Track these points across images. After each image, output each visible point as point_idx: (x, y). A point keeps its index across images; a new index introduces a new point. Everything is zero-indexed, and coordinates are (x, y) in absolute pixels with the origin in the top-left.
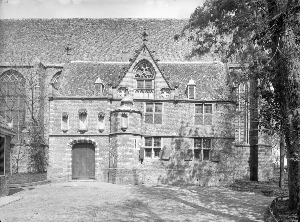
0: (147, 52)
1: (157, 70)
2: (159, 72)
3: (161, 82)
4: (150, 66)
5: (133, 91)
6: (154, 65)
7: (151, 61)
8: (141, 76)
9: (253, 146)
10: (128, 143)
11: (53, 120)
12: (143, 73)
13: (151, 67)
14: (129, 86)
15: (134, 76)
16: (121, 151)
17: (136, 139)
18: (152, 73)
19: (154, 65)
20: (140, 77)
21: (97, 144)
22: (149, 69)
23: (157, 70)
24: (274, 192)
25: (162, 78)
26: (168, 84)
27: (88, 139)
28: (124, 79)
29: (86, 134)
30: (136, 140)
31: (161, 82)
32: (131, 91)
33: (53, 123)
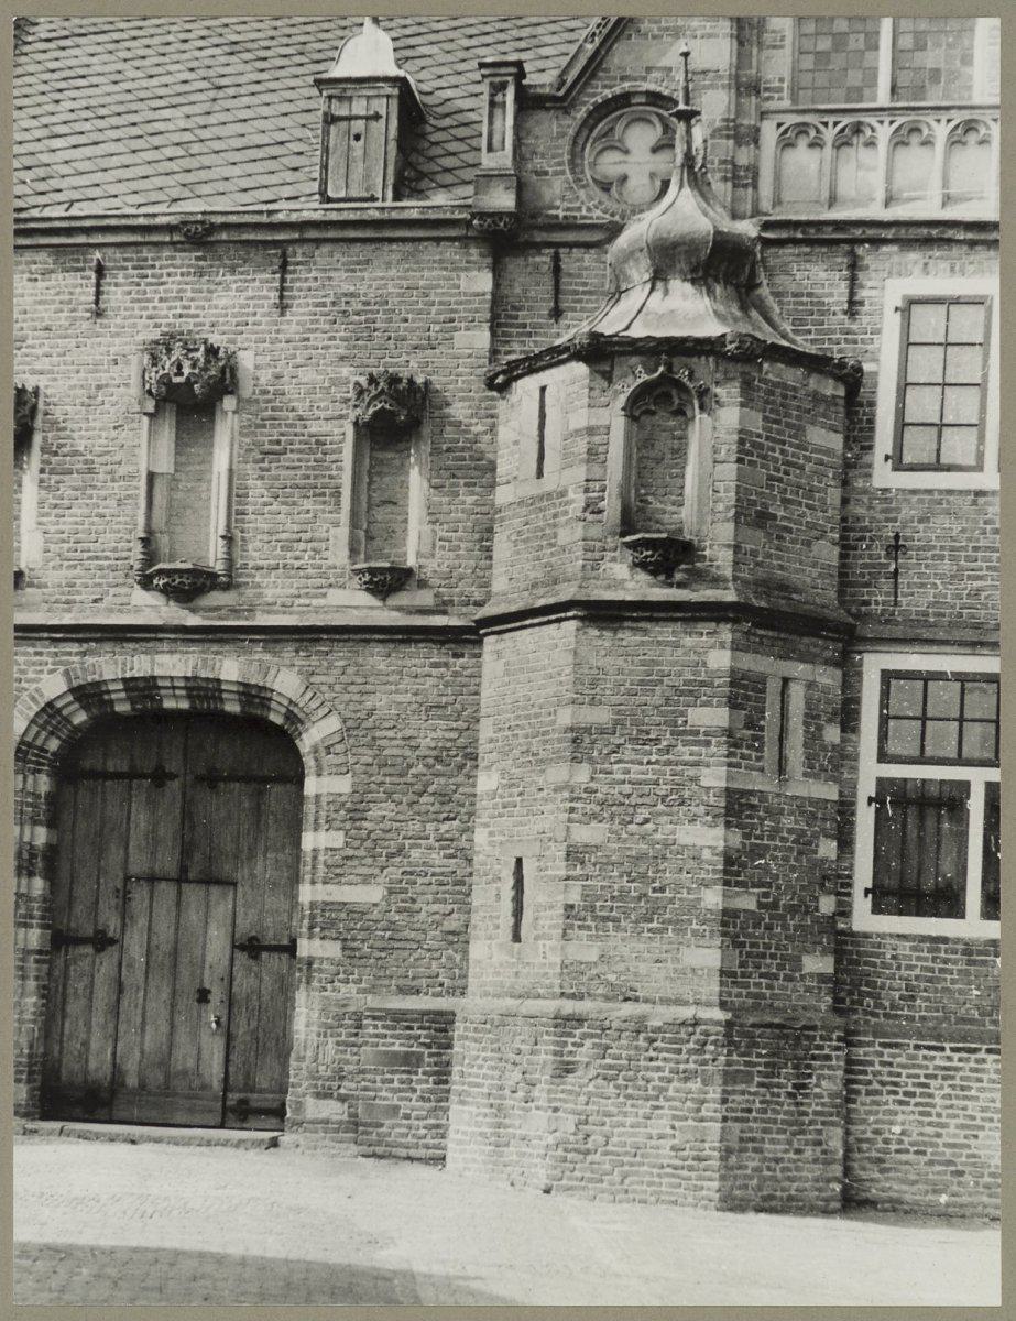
5: (754, 137)
29: (215, 608)
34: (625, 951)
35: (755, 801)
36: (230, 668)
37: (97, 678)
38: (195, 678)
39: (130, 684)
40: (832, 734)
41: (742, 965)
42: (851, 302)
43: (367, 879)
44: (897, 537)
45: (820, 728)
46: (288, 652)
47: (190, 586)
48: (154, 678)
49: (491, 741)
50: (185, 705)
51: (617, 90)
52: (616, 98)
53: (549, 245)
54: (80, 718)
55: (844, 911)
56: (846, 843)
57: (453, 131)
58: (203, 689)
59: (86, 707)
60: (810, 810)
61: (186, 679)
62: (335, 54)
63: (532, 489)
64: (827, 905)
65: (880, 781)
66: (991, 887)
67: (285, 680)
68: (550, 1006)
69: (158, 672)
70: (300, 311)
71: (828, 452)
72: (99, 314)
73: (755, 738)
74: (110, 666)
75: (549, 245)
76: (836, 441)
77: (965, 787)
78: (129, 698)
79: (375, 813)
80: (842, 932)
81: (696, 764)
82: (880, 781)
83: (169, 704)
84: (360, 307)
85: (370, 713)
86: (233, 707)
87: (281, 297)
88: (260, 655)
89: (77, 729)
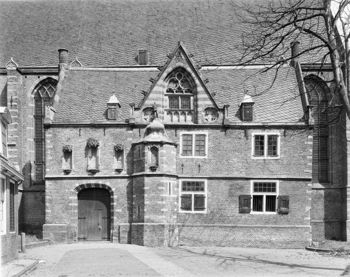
1: (197, 82)
6: (193, 75)
8: (175, 91)
10: (160, 188)
12: (178, 86)
14: (158, 106)
15: (165, 90)
16: (150, 199)
18: (190, 86)
19: (193, 75)
20: (173, 92)
23: (197, 82)
29: (97, 175)
31: (205, 99)
34: (152, 217)
35: (166, 198)
36: (100, 182)
37: (83, 184)
38: (96, 184)
39: (87, 184)
40: (176, 189)
41: (166, 218)
42: (176, 135)
43: (119, 208)
44: (183, 164)
45: (174, 188)
46: (108, 180)
47: (93, 172)
48: (90, 184)
49: (134, 191)
50: (94, 187)
51: (147, 107)
52: (146, 108)
53: (139, 127)
54: (81, 189)
55: (178, 210)
56: (178, 202)
57: (125, 109)
58: (97, 185)
59: (81, 188)
60: (174, 198)
61: (95, 184)
62: (109, 98)
63: (138, 159)
64: (176, 210)
65: (266, 211)
66: (303, 102)
67: (108, 183)
68: (144, 224)
69: (91, 183)
70: (107, 136)
71: (174, 154)
72: (80, 135)
73: (167, 190)
74: (85, 182)
75: (139, 127)
76: (175, 153)
77: (191, 195)
78: (87, 186)
79: (120, 200)
80: (178, 213)
81: (160, 194)
82: (266, 211)
83: (92, 187)
84: (115, 135)
85: (119, 187)
86: (101, 187)
87: (104, 133)
88: (104, 180)
89: (80, 190)
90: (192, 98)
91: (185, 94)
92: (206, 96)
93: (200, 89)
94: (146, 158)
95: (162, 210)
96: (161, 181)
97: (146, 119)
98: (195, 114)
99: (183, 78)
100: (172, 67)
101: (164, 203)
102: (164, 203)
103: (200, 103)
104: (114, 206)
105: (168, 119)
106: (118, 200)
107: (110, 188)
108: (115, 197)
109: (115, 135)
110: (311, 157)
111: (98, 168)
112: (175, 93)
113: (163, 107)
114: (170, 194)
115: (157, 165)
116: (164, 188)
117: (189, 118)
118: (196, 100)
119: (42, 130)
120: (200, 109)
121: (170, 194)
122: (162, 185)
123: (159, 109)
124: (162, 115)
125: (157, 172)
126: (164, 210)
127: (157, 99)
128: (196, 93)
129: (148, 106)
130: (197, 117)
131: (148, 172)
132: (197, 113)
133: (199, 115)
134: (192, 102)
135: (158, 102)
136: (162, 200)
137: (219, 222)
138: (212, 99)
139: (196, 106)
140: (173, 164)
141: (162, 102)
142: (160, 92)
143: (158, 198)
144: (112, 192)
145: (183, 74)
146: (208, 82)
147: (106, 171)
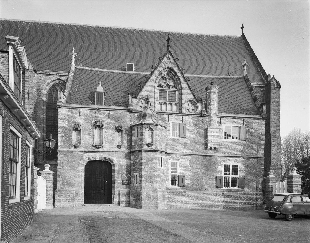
0: (172, 60)
1: (182, 80)
2: (185, 82)
3: (188, 94)
4: (174, 75)
6: (179, 74)
7: (176, 70)
9: (281, 165)
10: (155, 161)
11: (63, 132)
13: (174, 76)
14: (151, 97)
15: (156, 85)
16: (147, 171)
17: (163, 157)
18: (175, 83)
19: (179, 74)
20: (162, 87)
21: (115, 162)
22: (173, 79)
23: (182, 80)
24: (153, 84)
25: (191, 95)
26: (194, 96)
27: (105, 155)
28: (145, 88)
29: (100, 150)
30: (137, 176)
31: (188, 94)
32: (153, 102)
33: (62, 137)
50: (99, 160)
90: (177, 93)
91: (172, 89)
92: (189, 91)
93: (184, 85)
94: (143, 137)
95: (156, 179)
96: (156, 156)
97: (141, 107)
98: (180, 105)
99: (170, 77)
100: (162, 67)
101: (158, 173)
102: (158, 173)
103: (183, 96)
104: (115, 176)
105: (158, 107)
106: (118, 171)
107: (112, 161)
108: (116, 168)
109: (116, 118)
110: (264, 142)
111: (102, 144)
112: (164, 88)
113: (155, 98)
114: (162, 167)
115: (153, 143)
116: (158, 161)
117: (174, 108)
118: (180, 94)
119: (162, 59)
120: (183, 101)
121: (162, 167)
122: (156, 159)
123: (152, 100)
124: (154, 104)
125: (153, 147)
126: (158, 179)
127: (151, 92)
128: (181, 89)
129: (143, 97)
130: (182, 107)
131: (146, 147)
132: (181, 104)
133: (183, 106)
134: (177, 96)
135: (151, 94)
136: (156, 171)
137: (197, 190)
138: (193, 94)
139: (181, 99)
140: (163, 143)
141: (154, 94)
142: (152, 86)
143: (153, 169)
144: (114, 165)
145: (170, 74)
146: (190, 80)
147: (108, 147)
